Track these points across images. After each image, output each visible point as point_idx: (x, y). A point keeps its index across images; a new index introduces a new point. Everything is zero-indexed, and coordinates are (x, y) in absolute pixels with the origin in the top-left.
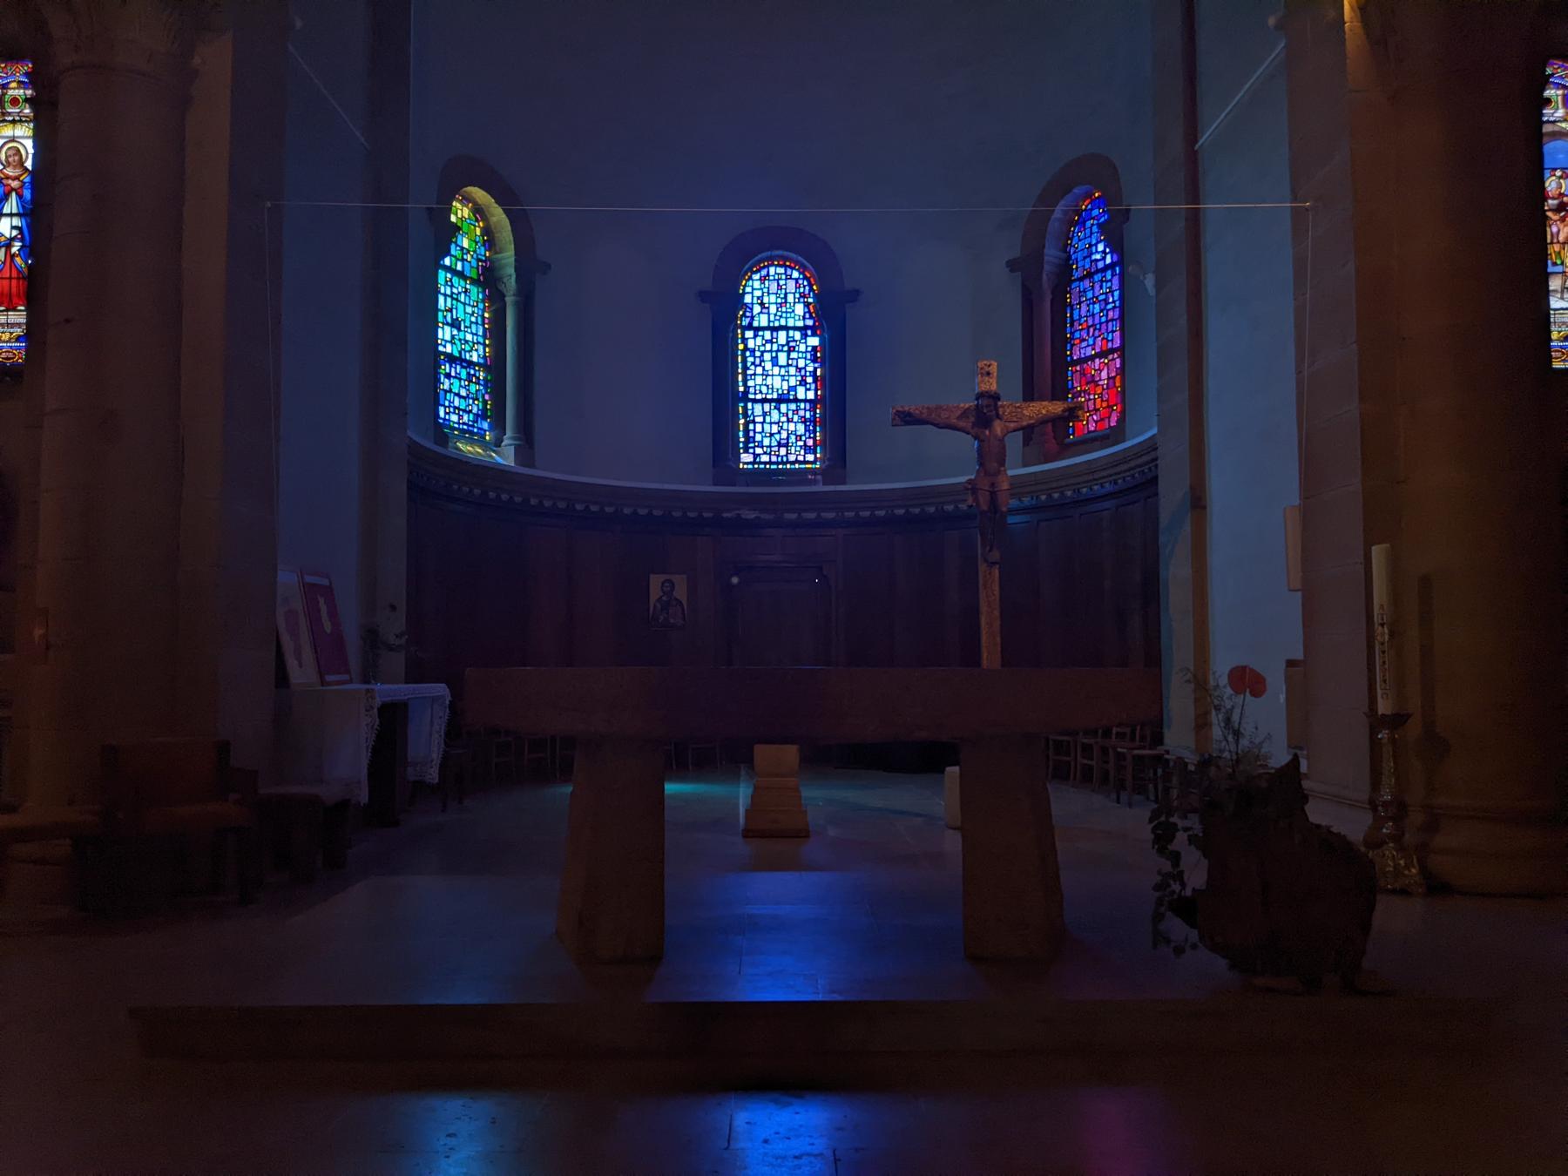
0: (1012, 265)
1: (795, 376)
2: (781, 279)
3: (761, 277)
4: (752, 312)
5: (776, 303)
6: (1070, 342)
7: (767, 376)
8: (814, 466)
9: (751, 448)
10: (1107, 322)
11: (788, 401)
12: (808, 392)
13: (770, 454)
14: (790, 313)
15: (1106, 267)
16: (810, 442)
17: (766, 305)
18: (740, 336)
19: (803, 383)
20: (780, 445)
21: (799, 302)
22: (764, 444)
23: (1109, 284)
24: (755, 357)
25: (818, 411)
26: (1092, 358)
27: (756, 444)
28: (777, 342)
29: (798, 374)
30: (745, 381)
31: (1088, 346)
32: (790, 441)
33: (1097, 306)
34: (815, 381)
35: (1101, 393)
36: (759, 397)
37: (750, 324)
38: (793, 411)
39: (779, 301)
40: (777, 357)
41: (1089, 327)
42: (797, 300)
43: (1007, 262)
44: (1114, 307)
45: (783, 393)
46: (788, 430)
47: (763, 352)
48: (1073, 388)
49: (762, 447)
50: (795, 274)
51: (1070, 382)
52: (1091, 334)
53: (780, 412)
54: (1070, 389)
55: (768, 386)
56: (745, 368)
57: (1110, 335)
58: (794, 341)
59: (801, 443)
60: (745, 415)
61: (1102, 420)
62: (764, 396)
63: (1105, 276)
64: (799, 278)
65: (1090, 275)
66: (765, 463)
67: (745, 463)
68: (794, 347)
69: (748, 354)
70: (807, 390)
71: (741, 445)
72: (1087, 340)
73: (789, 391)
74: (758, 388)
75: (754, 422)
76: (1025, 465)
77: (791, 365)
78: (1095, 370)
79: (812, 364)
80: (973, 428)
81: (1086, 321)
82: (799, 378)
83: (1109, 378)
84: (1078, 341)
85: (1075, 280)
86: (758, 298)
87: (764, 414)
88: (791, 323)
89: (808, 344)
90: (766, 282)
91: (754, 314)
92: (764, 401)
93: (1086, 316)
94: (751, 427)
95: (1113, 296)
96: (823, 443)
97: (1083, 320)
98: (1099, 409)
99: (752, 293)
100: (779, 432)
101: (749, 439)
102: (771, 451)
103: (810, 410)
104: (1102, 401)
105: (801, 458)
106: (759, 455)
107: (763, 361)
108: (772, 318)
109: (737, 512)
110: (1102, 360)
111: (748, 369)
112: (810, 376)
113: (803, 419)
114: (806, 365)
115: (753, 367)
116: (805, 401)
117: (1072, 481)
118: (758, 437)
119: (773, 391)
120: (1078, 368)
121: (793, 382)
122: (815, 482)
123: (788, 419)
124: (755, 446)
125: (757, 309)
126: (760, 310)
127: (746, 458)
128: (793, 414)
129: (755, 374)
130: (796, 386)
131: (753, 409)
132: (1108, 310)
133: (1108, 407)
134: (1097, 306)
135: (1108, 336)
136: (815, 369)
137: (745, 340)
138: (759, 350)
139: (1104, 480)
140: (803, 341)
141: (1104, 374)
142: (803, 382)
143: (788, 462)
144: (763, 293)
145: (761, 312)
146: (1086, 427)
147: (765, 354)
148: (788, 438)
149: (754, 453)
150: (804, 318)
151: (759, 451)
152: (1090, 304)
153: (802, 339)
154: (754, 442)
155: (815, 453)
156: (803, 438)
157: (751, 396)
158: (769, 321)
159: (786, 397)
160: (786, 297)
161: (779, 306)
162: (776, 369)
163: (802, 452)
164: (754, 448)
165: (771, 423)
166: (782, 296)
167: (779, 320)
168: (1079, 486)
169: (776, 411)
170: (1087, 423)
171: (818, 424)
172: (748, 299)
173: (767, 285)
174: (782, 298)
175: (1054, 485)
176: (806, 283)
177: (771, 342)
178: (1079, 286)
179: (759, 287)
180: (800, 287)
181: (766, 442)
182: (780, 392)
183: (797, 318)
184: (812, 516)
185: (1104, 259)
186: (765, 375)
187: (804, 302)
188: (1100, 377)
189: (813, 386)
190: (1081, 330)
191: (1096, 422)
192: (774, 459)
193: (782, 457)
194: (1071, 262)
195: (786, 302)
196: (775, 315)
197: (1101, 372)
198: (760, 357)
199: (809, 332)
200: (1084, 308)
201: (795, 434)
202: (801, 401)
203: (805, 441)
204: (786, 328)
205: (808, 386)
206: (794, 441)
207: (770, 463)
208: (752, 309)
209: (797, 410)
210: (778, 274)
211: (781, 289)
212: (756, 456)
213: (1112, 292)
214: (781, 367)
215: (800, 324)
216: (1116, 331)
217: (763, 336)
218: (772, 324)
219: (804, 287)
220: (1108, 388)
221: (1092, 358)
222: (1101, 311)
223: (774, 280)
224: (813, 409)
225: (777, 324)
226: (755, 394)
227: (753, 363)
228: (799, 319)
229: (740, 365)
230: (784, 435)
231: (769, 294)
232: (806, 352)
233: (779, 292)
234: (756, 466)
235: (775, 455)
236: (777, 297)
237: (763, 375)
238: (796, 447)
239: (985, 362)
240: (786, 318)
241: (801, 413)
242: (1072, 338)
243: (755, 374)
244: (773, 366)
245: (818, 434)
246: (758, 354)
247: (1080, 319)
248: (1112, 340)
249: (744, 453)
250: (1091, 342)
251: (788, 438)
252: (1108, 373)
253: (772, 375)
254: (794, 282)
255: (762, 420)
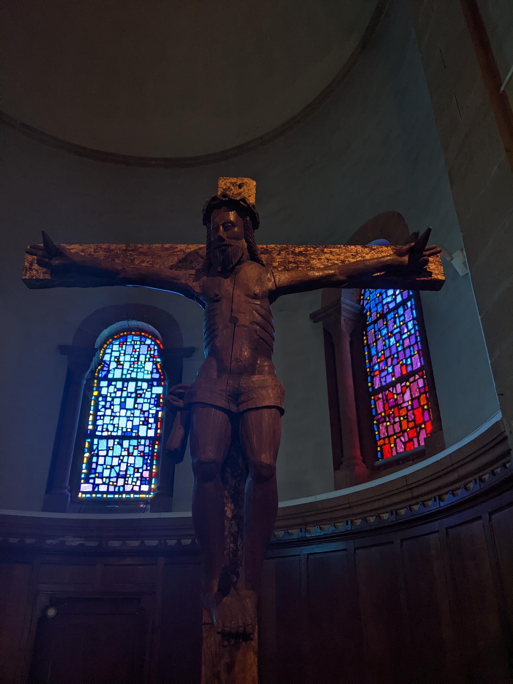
0: (315, 317)
1: (140, 417)
2: (136, 344)
3: (120, 342)
4: (109, 368)
5: (130, 361)
6: (370, 375)
7: (114, 417)
8: (147, 496)
9: (92, 478)
10: (404, 349)
11: (130, 438)
12: (149, 430)
13: (108, 485)
14: (141, 368)
15: (397, 306)
16: (146, 474)
17: (122, 363)
18: (95, 385)
19: (146, 423)
20: (118, 476)
21: (149, 361)
22: (104, 475)
23: (402, 318)
24: (106, 402)
25: (156, 447)
26: (393, 385)
27: (97, 475)
28: (127, 390)
29: (142, 416)
30: (95, 420)
31: (388, 374)
32: (128, 473)
33: (392, 340)
34: (156, 422)
35: (407, 415)
36: (105, 434)
37: (106, 375)
38: (134, 446)
39: (133, 359)
40: (125, 402)
41: (386, 359)
42: (147, 360)
43: (311, 315)
44: (409, 336)
45: (127, 431)
46: (127, 463)
47: (113, 398)
48: (377, 414)
49: (102, 478)
50: (148, 342)
51: (374, 410)
52: (389, 364)
53: (122, 447)
54: (375, 416)
55: (114, 425)
56: (97, 410)
57: (409, 360)
58: (142, 389)
59: (138, 475)
60: (91, 450)
61: (411, 440)
62: (109, 433)
63: (398, 313)
64: (151, 344)
65: (383, 316)
66: (103, 493)
67: (84, 493)
68: (141, 394)
69: (100, 399)
70: (149, 428)
71: (83, 476)
72: (387, 370)
73: (132, 429)
74: (105, 426)
75: (98, 456)
76: (337, 488)
77: (137, 409)
78: (397, 394)
79: (155, 408)
80: (197, 277)
81: (384, 354)
82: (143, 419)
83: (412, 399)
84: (377, 373)
85: (370, 324)
86: (116, 357)
87: (108, 449)
88: (140, 376)
89: (153, 392)
90: (124, 346)
91: (111, 368)
92: (108, 438)
93: (384, 350)
94: (95, 459)
95: (407, 327)
96: (156, 475)
97: (380, 354)
98: (406, 430)
99: (111, 354)
100: (119, 465)
101: (91, 470)
102: (110, 481)
103: (148, 446)
104: (408, 422)
105: (136, 489)
106: (98, 485)
107: (113, 405)
108: (125, 372)
109: (62, 539)
110: (403, 384)
111: (99, 411)
112: (153, 417)
113: (142, 454)
114: (150, 409)
115: (103, 410)
116: (146, 438)
117: (388, 502)
118: (99, 469)
119: (118, 429)
120: (380, 396)
121: (136, 422)
122: (144, 510)
123: (129, 453)
124: (96, 477)
125: (113, 365)
126: (115, 366)
127: (86, 487)
128: (134, 449)
129: (104, 415)
130: (139, 426)
131: (98, 445)
132: (403, 340)
133: (416, 426)
134: (392, 340)
135: (406, 361)
136: (157, 412)
137: (99, 389)
138: (110, 397)
139: (426, 497)
140: (149, 390)
141: (407, 396)
142: (146, 422)
143: (124, 492)
144: (120, 353)
145: (117, 368)
146: (394, 450)
147: (115, 400)
148: (126, 471)
149: (94, 484)
150: (152, 373)
151: (98, 481)
152: (386, 339)
153: (148, 388)
154: (95, 473)
155: (150, 484)
156: (141, 470)
157: (98, 433)
158: (122, 374)
159: (129, 434)
160: (138, 357)
161: (132, 363)
162: (123, 412)
163: (138, 483)
164: (94, 479)
165: (113, 457)
166: (136, 356)
167: (131, 374)
168: (397, 507)
169: (119, 446)
170: (395, 446)
171: (155, 458)
172: (107, 358)
173: (124, 348)
174: (135, 358)
175: (369, 507)
176: (156, 348)
177: (122, 390)
178: (374, 328)
179: (117, 349)
180: (151, 350)
181: (106, 473)
182: (124, 430)
183: (146, 372)
184: (135, 544)
185: (395, 300)
186: (113, 416)
187: (153, 361)
188: (403, 400)
189: (154, 426)
190: (379, 363)
191: (405, 443)
192: (111, 489)
193: (119, 487)
194: (365, 311)
195: (138, 361)
196: (128, 370)
197: (403, 395)
198: (110, 402)
199: (155, 383)
200: (380, 343)
201: (134, 467)
202: (142, 438)
203: (142, 473)
204: (136, 380)
205: (150, 426)
206: (132, 473)
207: (108, 492)
208: (109, 365)
209: (138, 446)
210: (134, 341)
211: (135, 352)
212: (95, 485)
213: (406, 324)
214: (127, 410)
215: (149, 377)
216: (415, 355)
217: (115, 386)
218: (124, 377)
219: (155, 350)
220: (413, 409)
221: (393, 385)
222: (397, 342)
223: (131, 345)
224: (152, 445)
225: (128, 376)
226: (102, 431)
227: (104, 407)
228: (148, 373)
229: (92, 408)
230: (123, 467)
231: (125, 354)
232: (151, 398)
233: (134, 353)
234: (94, 495)
235: (113, 485)
236: (131, 357)
237: (111, 416)
238: (133, 478)
239: (233, 180)
240: (137, 372)
241: (141, 448)
242: (372, 371)
243: (104, 415)
244: (121, 409)
245: (154, 467)
246: (109, 399)
247: (377, 354)
248: (412, 364)
249: (84, 483)
250: (390, 370)
251: (126, 471)
252: (411, 395)
253: (120, 416)
254: (147, 346)
255: (105, 454)
